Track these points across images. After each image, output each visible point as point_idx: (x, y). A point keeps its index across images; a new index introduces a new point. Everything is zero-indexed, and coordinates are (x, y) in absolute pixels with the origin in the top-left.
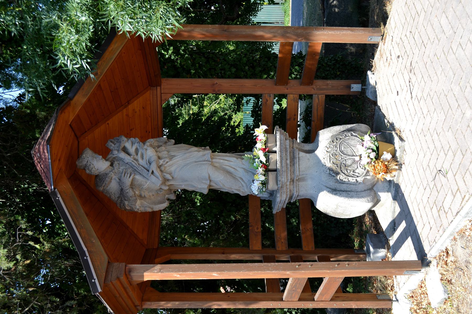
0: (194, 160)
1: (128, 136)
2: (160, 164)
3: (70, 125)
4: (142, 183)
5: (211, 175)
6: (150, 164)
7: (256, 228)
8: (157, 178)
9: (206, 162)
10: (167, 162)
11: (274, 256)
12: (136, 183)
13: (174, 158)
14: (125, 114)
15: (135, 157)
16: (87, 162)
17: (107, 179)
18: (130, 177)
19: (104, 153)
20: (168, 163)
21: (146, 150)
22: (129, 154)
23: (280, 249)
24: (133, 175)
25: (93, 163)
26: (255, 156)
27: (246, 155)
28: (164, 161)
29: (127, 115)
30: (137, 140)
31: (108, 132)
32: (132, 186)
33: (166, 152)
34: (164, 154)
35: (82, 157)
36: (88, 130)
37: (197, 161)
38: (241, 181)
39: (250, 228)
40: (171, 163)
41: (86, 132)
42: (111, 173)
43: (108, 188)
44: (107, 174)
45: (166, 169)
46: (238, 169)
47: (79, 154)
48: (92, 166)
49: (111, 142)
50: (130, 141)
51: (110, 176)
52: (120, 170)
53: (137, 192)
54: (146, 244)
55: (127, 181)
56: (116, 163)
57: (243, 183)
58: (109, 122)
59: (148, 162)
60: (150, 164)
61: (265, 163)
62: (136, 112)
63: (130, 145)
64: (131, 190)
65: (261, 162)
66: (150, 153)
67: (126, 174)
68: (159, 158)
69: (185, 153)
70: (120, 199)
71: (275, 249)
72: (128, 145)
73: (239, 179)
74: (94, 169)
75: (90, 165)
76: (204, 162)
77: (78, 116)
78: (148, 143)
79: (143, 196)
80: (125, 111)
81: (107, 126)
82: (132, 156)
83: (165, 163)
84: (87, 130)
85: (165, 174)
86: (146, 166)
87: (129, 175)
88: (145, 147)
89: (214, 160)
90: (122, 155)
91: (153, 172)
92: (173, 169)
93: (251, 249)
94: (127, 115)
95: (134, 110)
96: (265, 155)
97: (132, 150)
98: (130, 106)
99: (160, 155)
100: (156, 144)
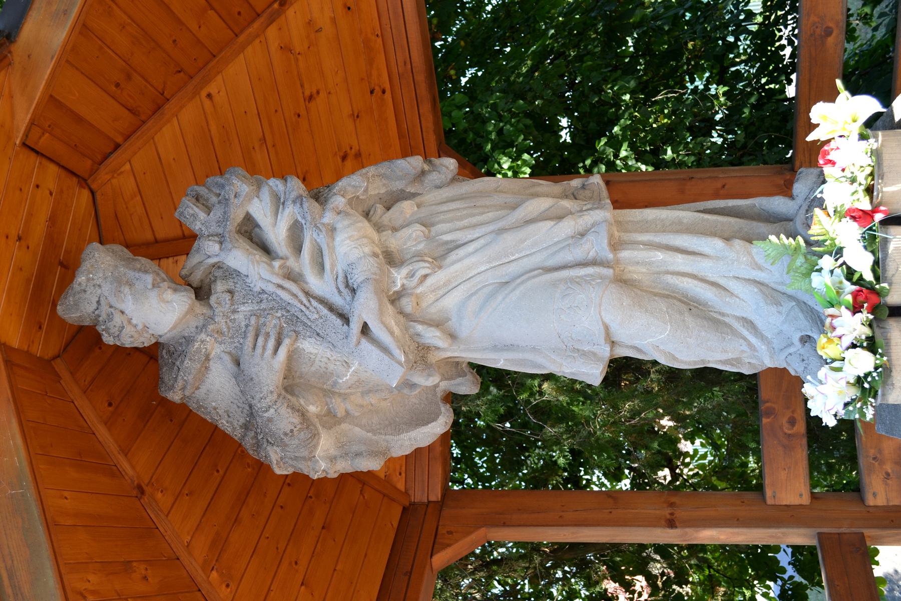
0: (537, 260)
1: (256, 171)
2: (398, 287)
3: (24, 144)
4: (331, 367)
5: (614, 327)
6: (354, 291)
7: (784, 421)
8: (385, 350)
9: (590, 270)
10: (425, 276)
11: (862, 537)
12: (304, 369)
13: (453, 256)
14: (274, 46)
15: (292, 263)
16: (98, 302)
17: (187, 363)
18: (276, 351)
19: (166, 249)
20: (429, 281)
21: (332, 230)
22: (265, 249)
23: (881, 501)
24: (287, 342)
25: (122, 306)
26: (819, 243)
27: (773, 238)
28: (411, 275)
29: (286, 48)
30: (295, 185)
31: (213, 128)
32: (292, 385)
33: (416, 230)
34: (410, 239)
35: (75, 285)
36: (127, 138)
37: (551, 263)
38: (745, 333)
39: (765, 421)
40: (440, 277)
41: (117, 146)
42: (203, 336)
43: (201, 393)
44: (189, 340)
45: (424, 305)
46: (732, 285)
47: (68, 267)
48: (118, 319)
49: (198, 198)
50: (265, 193)
51: (199, 350)
52: (240, 317)
53: (313, 409)
54: (402, 488)
55: (268, 369)
56: (219, 287)
57: (753, 340)
58: (212, 88)
59: (342, 287)
60: (354, 291)
61: (869, 277)
62: (319, 30)
63: (270, 206)
64: (284, 410)
65: (850, 274)
66: (350, 245)
67: (261, 340)
68: (391, 259)
69: (502, 231)
70: (252, 434)
71: (862, 500)
72: (260, 209)
73: (737, 325)
74: (128, 330)
75: (110, 317)
76: (582, 272)
77: (52, 101)
78: (338, 201)
79: (340, 413)
80: (272, 32)
81: (207, 103)
82: (277, 264)
83: (416, 280)
84: (119, 140)
85: (420, 328)
86: (338, 301)
87: (271, 343)
88: (329, 218)
89: (625, 254)
90: (239, 258)
91: (365, 329)
92: (450, 302)
93: (769, 501)
94: (286, 48)
95: (310, 23)
96: (870, 241)
97: (276, 233)
98: (290, 12)
99: (394, 242)
100: (378, 188)
